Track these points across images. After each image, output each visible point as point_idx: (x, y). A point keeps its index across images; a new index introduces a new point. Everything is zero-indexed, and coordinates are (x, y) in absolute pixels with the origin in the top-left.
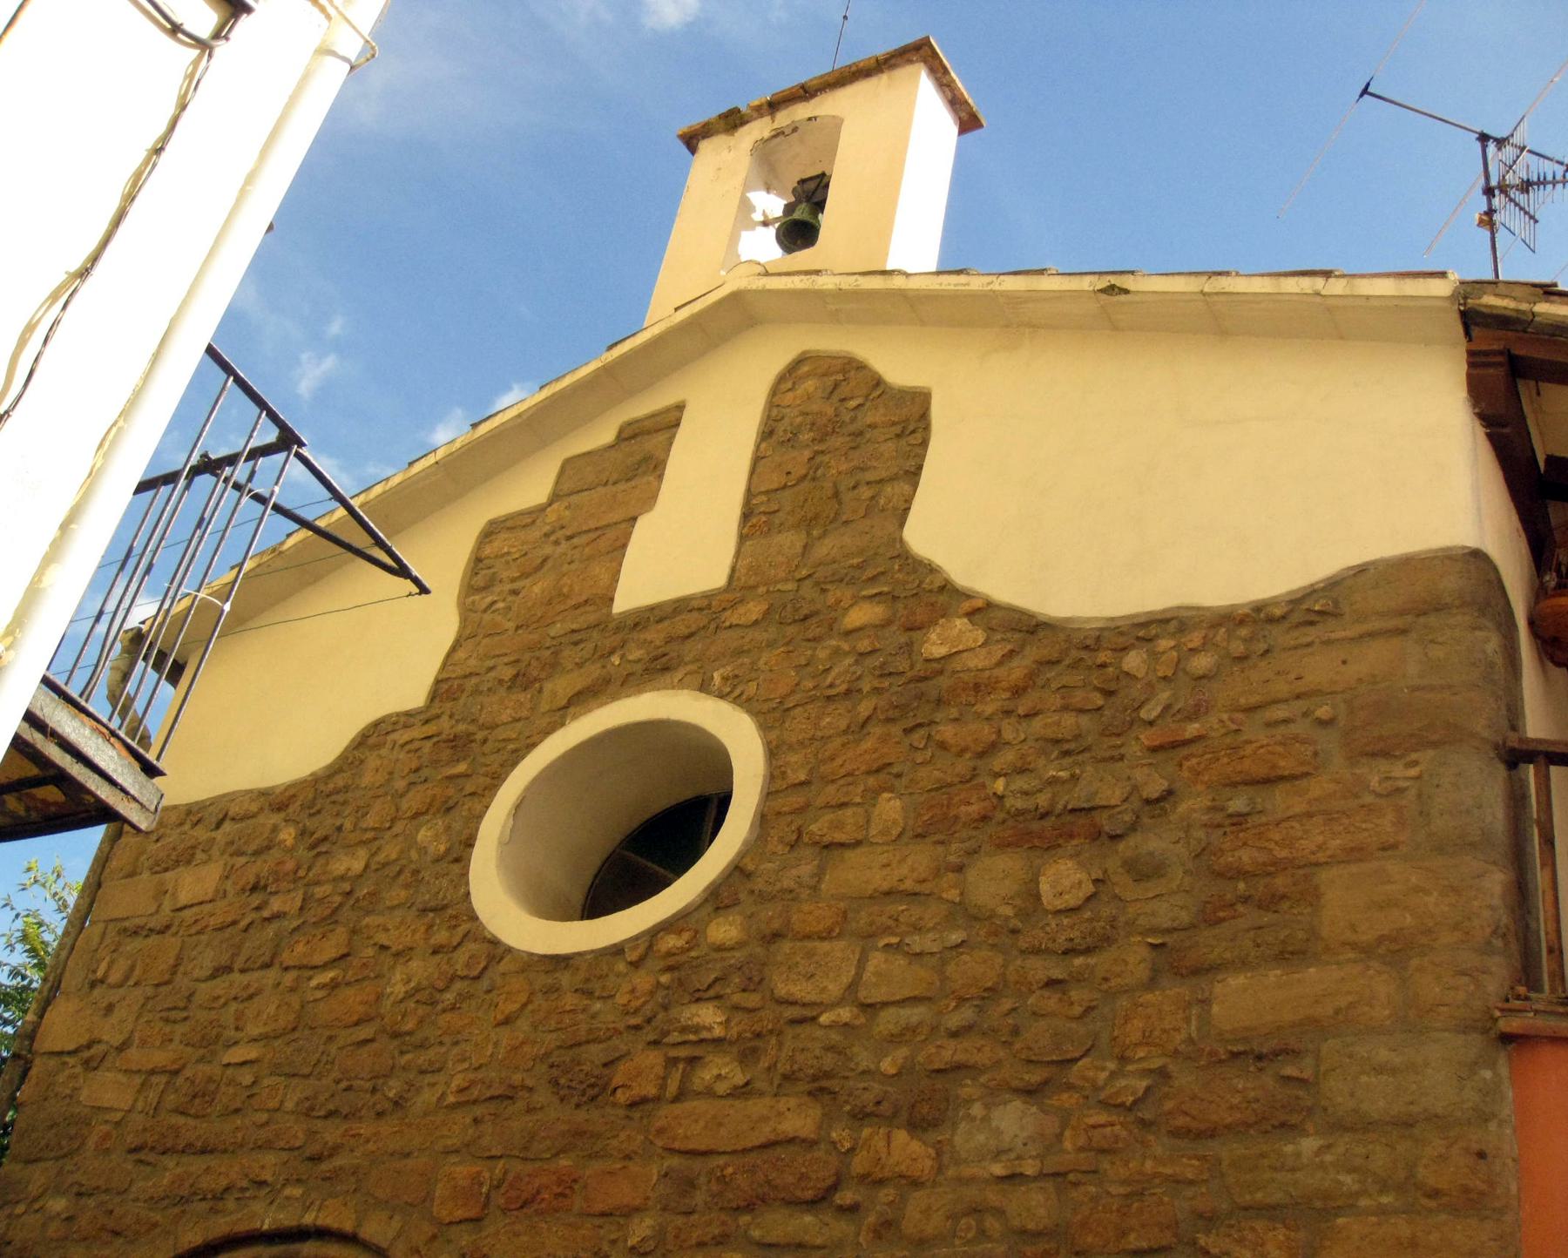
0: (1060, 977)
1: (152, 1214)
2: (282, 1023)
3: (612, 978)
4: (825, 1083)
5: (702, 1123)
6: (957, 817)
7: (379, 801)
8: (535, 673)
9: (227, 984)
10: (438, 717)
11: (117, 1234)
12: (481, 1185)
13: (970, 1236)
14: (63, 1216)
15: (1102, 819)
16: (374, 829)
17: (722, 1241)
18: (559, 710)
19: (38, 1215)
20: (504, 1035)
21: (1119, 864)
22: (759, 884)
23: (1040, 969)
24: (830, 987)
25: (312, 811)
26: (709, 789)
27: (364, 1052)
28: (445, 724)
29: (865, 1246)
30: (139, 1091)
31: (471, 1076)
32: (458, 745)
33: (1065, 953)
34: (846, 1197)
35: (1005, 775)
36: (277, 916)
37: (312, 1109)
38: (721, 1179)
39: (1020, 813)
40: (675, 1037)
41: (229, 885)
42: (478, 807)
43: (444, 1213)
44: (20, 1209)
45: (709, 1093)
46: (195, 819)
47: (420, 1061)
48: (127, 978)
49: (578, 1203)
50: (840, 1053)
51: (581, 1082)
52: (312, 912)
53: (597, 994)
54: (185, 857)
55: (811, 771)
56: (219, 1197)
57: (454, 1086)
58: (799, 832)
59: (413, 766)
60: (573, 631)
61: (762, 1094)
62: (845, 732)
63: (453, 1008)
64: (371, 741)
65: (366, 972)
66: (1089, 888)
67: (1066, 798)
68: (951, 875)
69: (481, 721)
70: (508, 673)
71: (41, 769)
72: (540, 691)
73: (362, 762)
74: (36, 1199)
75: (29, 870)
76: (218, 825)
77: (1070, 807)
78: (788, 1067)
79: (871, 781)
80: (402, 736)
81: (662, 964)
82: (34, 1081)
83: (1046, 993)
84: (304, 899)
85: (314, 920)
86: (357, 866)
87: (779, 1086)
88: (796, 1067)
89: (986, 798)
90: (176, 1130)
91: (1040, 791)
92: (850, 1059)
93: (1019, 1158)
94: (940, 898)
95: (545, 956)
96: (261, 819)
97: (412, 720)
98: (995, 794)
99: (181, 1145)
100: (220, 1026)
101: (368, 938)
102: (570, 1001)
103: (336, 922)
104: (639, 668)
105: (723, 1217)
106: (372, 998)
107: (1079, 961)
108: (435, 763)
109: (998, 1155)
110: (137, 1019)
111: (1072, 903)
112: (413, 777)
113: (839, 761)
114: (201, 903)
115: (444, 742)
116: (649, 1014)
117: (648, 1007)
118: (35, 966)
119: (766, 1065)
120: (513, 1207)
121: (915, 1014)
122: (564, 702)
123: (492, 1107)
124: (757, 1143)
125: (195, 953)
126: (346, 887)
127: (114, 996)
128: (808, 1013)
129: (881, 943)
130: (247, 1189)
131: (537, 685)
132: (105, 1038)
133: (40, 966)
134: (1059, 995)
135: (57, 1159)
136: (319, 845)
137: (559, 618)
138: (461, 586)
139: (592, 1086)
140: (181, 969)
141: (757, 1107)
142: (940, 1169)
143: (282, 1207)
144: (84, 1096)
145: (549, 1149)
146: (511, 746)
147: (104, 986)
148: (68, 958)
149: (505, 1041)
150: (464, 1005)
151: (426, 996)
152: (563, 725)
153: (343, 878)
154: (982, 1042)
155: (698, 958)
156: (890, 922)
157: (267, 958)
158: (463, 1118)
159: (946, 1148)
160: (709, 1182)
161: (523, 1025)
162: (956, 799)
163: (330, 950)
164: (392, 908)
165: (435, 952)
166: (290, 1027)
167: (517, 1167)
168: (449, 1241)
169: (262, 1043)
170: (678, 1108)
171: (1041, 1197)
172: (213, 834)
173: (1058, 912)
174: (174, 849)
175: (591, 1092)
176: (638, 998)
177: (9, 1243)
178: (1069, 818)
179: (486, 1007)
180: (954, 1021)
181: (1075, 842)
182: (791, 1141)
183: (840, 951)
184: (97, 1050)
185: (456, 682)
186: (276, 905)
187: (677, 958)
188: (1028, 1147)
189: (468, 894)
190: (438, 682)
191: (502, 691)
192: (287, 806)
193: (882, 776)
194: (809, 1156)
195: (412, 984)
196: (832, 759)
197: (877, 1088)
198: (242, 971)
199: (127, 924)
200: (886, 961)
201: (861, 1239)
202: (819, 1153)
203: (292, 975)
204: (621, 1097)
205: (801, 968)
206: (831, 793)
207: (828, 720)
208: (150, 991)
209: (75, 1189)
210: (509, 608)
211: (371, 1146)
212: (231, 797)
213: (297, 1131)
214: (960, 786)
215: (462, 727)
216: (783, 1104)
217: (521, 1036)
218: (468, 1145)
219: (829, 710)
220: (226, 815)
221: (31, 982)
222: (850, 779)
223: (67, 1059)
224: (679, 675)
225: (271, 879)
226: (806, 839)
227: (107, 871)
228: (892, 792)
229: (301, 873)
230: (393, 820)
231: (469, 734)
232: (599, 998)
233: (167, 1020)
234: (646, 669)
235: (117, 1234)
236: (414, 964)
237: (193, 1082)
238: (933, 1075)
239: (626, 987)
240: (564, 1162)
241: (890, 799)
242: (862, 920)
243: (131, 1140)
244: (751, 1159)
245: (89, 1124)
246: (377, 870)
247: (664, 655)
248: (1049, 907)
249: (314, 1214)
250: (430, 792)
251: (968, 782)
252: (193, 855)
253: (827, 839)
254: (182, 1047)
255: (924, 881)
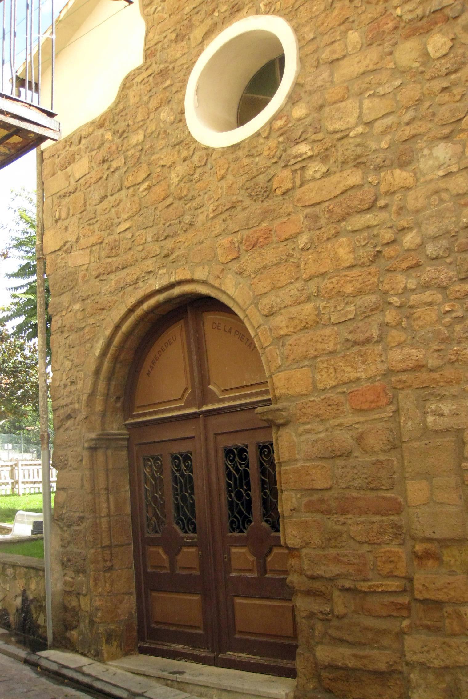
0: (447, 86)
1: (113, 298)
2: (134, 210)
3: (260, 146)
4: (359, 160)
5: (314, 192)
6: (383, 31)
7: (140, 109)
8: (184, 32)
9: (107, 202)
10: (151, 65)
11: (103, 309)
12: (234, 244)
13: (436, 203)
14: (81, 310)
15: (448, 11)
16: (142, 120)
17: (336, 235)
18: (200, 43)
19: (71, 313)
20: (224, 184)
21: (460, 29)
22: (308, 87)
23: (438, 85)
24: (350, 120)
25: (115, 122)
26: (274, 56)
27: (171, 208)
28: (155, 68)
29: (395, 220)
30: (90, 255)
31: (216, 204)
32: (163, 74)
33: (447, 75)
34: (381, 203)
35: (400, 6)
36: (117, 169)
37: (158, 238)
38: (330, 211)
39: (410, 21)
40: (293, 161)
41: (93, 164)
42: (181, 97)
43: (224, 259)
44: (64, 313)
45: (314, 179)
46: (69, 144)
47: (194, 205)
48: (68, 214)
49: (274, 238)
50: (362, 146)
51: (260, 192)
52: (130, 162)
53: (255, 155)
54: (71, 160)
55: (315, 33)
56: (136, 283)
57: (211, 211)
58: (318, 60)
59: (148, 89)
60: (194, 8)
61: (335, 173)
62: (325, 10)
63: (199, 180)
64: (127, 85)
65: (160, 178)
66: (450, 44)
67: (429, 7)
68: (388, 57)
69: (169, 60)
70: (173, 36)
71: (7, 130)
72: (189, 39)
73: (127, 95)
74: (68, 308)
75: (12, 192)
76: (80, 142)
77: (432, 11)
78: (343, 158)
79: (342, 28)
80: (139, 79)
81: (278, 133)
82: (49, 266)
83: (443, 94)
84: (125, 159)
85: (131, 165)
86: (141, 138)
87: (342, 167)
88: (346, 157)
89: (395, 18)
90: (110, 264)
91: (417, 8)
92: (368, 147)
93: (449, 166)
94: (386, 68)
95: (230, 147)
96: (96, 133)
97: (140, 71)
98: (397, 16)
99: (114, 268)
100: (111, 219)
101: (156, 165)
102: (245, 161)
103: (141, 163)
104: (227, 14)
105: (334, 226)
106: (166, 187)
107: (453, 77)
108: (157, 85)
109: (439, 167)
110: (78, 228)
111: (444, 52)
112: (150, 94)
113: (326, 24)
114: (85, 175)
115: (158, 74)
116: (279, 156)
117: (278, 153)
118: (30, 227)
119: (334, 160)
120: (250, 248)
121: (389, 120)
122: (201, 40)
123: (228, 213)
124: (339, 192)
125: (90, 195)
126: (140, 147)
127: (66, 223)
128: (344, 134)
129: (366, 96)
130: (145, 276)
131: (187, 37)
132: (69, 239)
133: (32, 226)
134: (448, 94)
135: (69, 290)
136: (122, 135)
137: (186, 4)
138: (140, 6)
139: (265, 192)
140: (88, 203)
141: (334, 179)
142: (417, 180)
143: (161, 279)
144: (70, 264)
145: (256, 222)
146: (185, 66)
147: (61, 220)
148: (43, 215)
149: (225, 186)
150: (203, 178)
151: (188, 178)
152: (203, 50)
153: (137, 145)
154: (421, 123)
155: (292, 126)
156: (368, 85)
157: (119, 187)
158: (219, 221)
159: (417, 171)
160: (324, 214)
161: (230, 177)
162: (381, 24)
163: (142, 175)
164: (161, 149)
165: (184, 161)
166: (138, 210)
167: (246, 233)
168: (230, 269)
169: (130, 220)
170: (303, 189)
171: (462, 179)
172: (79, 147)
173: (439, 58)
174: (66, 158)
175: (266, 194)
176: (272, 151)
177: (65, 326)
178: (433, 16)
179: (212, 175)
180: (407, 117)
181: (438, 25)
182: (353, 187)
183: (351, 104)
184: (68, 246)
185: (153, 48)
186: (114, 165)
187: (283, 129)
188: (452, 160)
189: (189, 132)
190: (146, 51)
191: (173, 45)
192: (104, 124)
193: (347, 24)
194: (361, 192)
195: (180, 177)
196: (322, 24)
197: (382, 155)
198: (112, 195)
199: (59, 194)
200: (371, 102)
201: (392, 217)
202: (366, 188)
203: (131, 190)
204: (279, 192)
205: (336, 117)
206: (326, 39)
207: (315, 8)
208: (79, 216)
209: (81, 299)
210: (163, 8)
211: (186, 244)
212: (80, 129)
213: (156, 248)
214: (381, 18)
215: (162, 66)
216: (345, 174)
217: (230, 182)
218: (224, 231)
219: (315, 3)
220: (81, 137)
221: (31, 233)
222: (332, 30)
223: (58, 253)
224: (245, 10)
225: (109, 156)
226: (321, 62)
227: (44, 176)
228: (352, 30)
229: (119, 149)
230: (148, 114)
231: (166, 68)
232: (257, 156)
233: (90, 225)
234: (231, 13)
235: (103, 309)
236: (178, 168)
237: (109, 244)
238: (404, 143)
239: (266, 148)
240: (264, 225)
241: (352, 33)
242: (355, 88)
243: (95, 274)
244: (338, 200)
245: (76, 274)
246: (149, 136)
247: (236, 5)
248: (435, 57)
249: (174, 277)
250: (159, 98)
251: (384, 14)
252: (74, 158)
253: (331, 59)
254: (99, 232)
255: (377, 63)
